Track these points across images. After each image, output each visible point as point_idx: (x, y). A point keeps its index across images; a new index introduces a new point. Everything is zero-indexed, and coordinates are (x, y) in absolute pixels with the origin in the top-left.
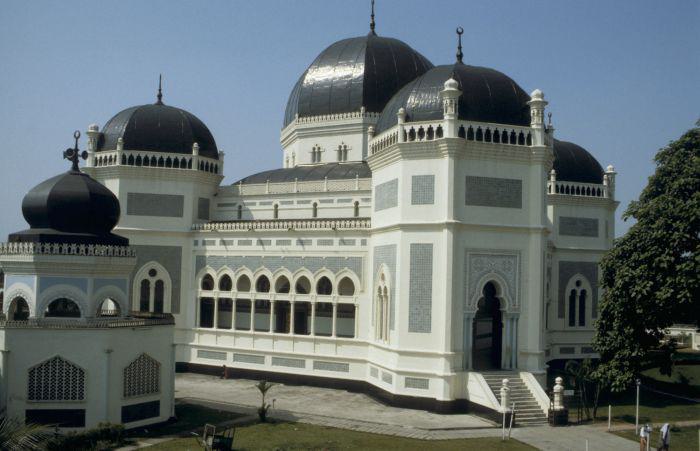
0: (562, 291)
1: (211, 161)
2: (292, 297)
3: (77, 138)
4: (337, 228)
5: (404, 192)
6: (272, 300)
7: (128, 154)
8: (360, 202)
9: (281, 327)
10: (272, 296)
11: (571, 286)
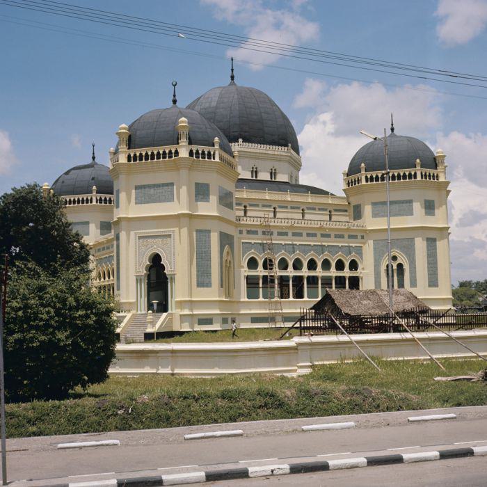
0: (377, 266)
2: (290, 272)
3: (175, 86)
8: (248, 205)
9: (284, 295)
10: (277, 272)
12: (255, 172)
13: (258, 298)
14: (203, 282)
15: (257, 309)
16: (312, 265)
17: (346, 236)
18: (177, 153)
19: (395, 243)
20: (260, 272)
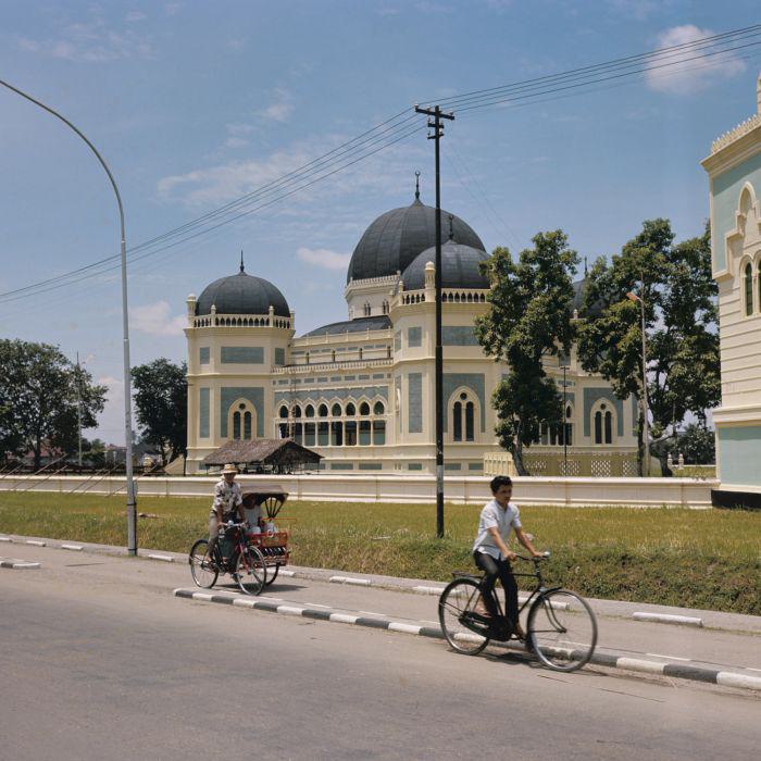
1: (283, 319)
2: (344, 418)
3: (418, 175)
4: (205, 392)
5: (269, 356)
6: (343, 421)
7: (220, 317)
9: (351, 441)
10: (330, 419)
11: (596, 408)
12: (368, 309)
13: (327, 444)
14: (415, 427)
15: (355, 455)
16: (365, 409)
17: (371, 377)
18: (423, 297)
19: (244, 392)
20: (291, 420)
